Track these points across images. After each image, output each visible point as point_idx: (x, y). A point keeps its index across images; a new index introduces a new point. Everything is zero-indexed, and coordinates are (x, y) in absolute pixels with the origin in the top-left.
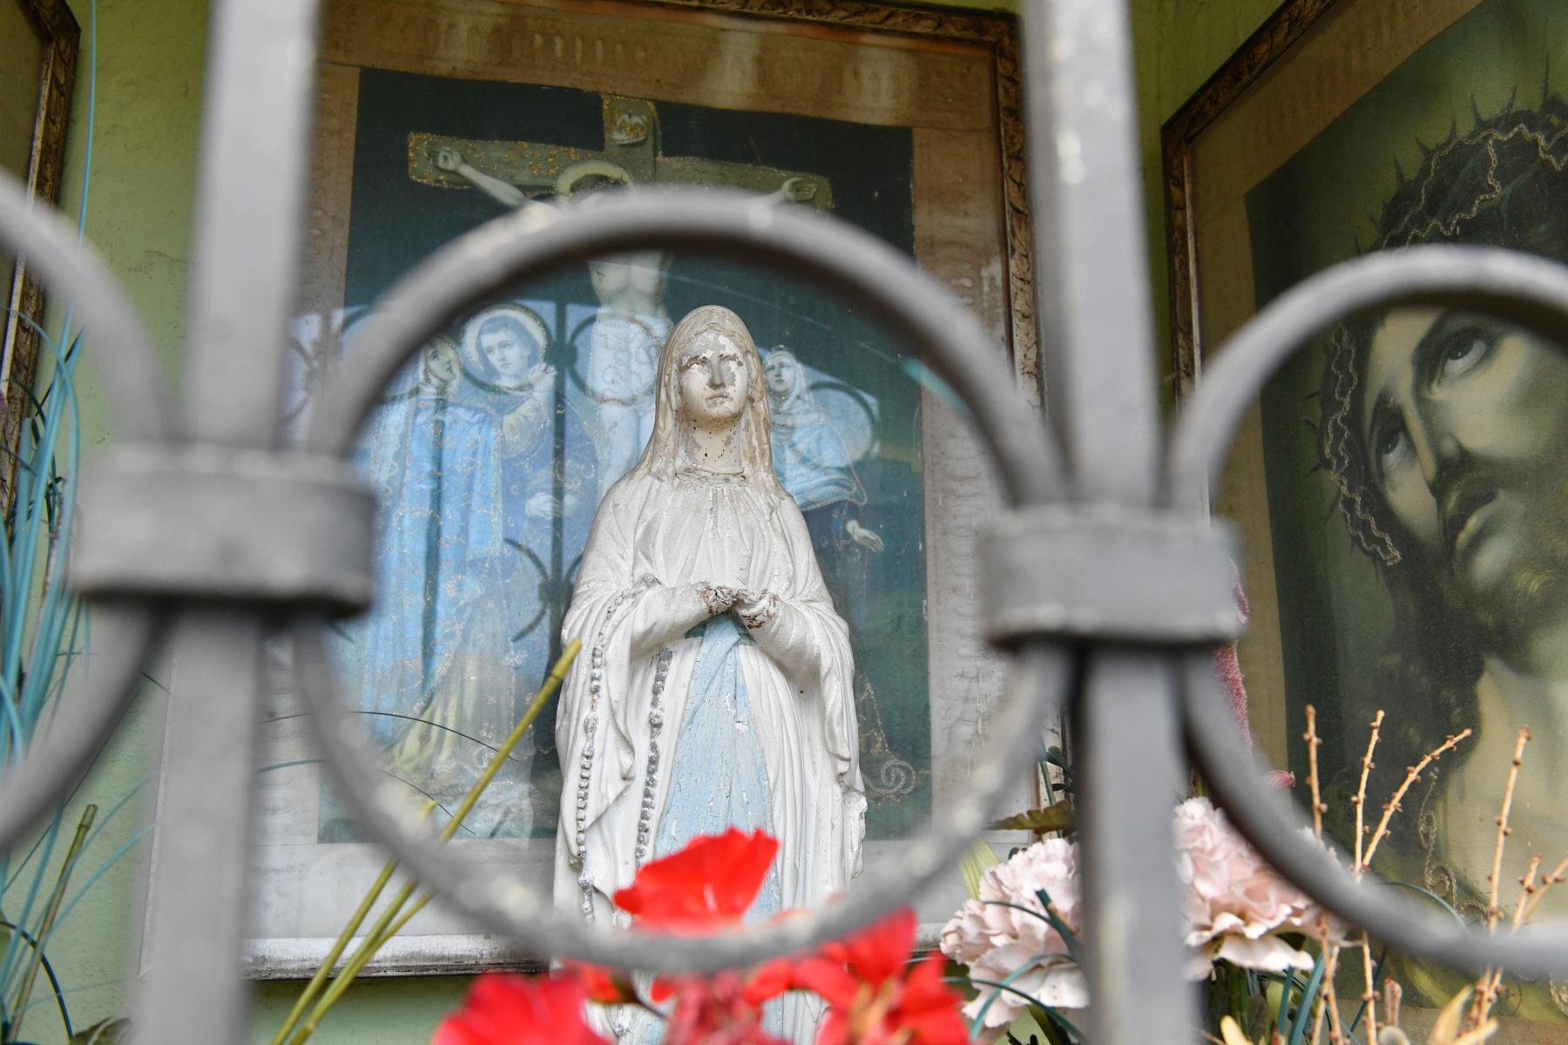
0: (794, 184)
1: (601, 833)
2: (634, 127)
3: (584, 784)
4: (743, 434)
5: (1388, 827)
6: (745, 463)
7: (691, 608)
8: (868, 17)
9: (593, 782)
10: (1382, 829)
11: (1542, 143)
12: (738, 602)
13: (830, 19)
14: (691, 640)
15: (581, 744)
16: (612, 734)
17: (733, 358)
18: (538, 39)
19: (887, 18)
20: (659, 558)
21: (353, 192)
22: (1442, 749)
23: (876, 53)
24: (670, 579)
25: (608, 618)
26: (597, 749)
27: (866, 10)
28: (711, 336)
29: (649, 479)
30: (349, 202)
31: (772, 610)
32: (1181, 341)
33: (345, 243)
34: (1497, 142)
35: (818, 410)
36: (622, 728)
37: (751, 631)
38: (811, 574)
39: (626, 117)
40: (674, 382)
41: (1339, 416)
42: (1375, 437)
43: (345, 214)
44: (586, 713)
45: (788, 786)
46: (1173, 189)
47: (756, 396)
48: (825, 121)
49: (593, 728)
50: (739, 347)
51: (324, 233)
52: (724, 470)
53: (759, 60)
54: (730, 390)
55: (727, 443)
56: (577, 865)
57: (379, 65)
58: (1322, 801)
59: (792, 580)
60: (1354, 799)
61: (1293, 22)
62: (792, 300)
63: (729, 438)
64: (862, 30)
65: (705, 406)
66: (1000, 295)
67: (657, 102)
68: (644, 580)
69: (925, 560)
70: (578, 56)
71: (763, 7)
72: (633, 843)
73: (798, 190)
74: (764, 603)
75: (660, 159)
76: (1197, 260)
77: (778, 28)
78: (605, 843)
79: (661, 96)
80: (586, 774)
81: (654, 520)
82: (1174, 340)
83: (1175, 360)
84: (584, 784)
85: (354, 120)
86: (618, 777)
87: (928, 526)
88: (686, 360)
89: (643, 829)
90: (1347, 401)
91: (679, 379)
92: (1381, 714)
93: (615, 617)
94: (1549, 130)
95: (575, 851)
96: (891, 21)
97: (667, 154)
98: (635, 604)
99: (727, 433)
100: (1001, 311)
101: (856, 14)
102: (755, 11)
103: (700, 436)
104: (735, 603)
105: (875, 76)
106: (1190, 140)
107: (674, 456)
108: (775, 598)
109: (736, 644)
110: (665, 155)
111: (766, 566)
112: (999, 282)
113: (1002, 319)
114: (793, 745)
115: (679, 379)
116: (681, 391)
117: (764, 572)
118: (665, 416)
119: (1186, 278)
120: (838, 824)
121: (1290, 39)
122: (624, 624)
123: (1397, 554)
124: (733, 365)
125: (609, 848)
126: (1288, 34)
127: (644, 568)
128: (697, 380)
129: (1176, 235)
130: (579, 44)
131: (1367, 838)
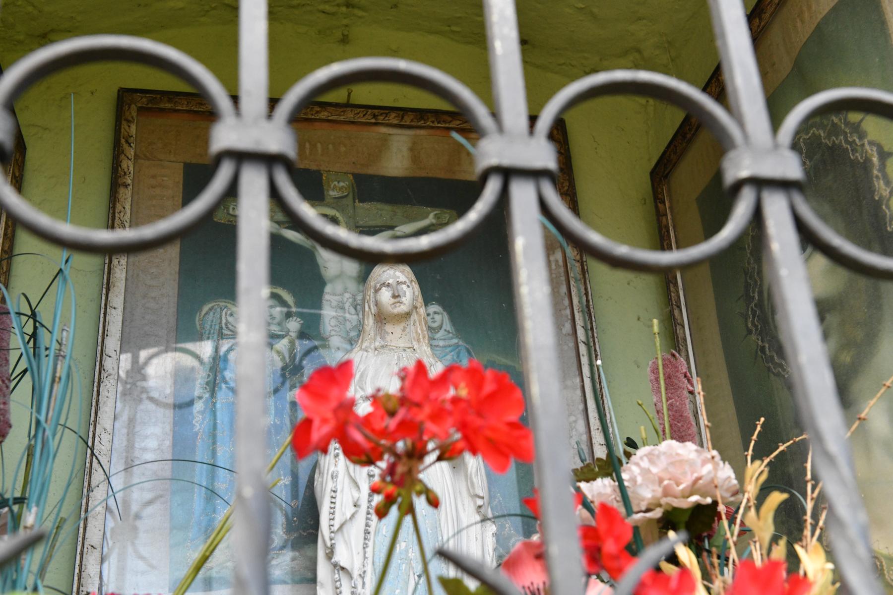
1: (343, 536)
2: (341, 189)
3: (333, 506)
6: (414, 343)
9: (338, 505)
15: (330, 485)
16: (347, 480)
17: (405, 283)
26: (339, 488)
29: (361, 352)
32: (672, 289)
34: (804, 139)
35: (457, 337)
36: (352, 474)
39: (336, 183)
40: (372, 299)
41: (753, 305)
44: (332, 469)
45: (448, 510)
47: (419, 305)
48: (452, 180)
49: (337, 476)
52: (402, 345)
53: (411, 149)
54: (403, 299)
55: (404, 330)
56: (330, 555)
57: (194, 161)
62: (438, 277)
65: (390, 309)
66: (562, 270)
67: (354, 175)
70: (308, 152)
71: (412, 121)
72: (362, 541)
73: (438, 218)
77: (422, 132)
78: (345, 541)
79: (356, 171)
80: (333, 500)
81: (365, 370)
82: (668, 289)
83: (670, 300)
84: (333, 506)
85: (181, 190)
86: (351, 505)
89: (367, 532)
92: (762, 419)
95: (329, 544)
97: (361, 201)
99: (402, 325)
100: (563, 278)
102: (408, 123)
103: (389, 328)
106: (666, 177)
107: (375, 340)
110: (360, 201)
112: (561, 263)
113: (564, 283)
114: (452, 496)
116: (377, 304)
120: (479, 538)
124: (404, 287)
125: (347, 543)
128: (385, 296)
130: (307, 145)
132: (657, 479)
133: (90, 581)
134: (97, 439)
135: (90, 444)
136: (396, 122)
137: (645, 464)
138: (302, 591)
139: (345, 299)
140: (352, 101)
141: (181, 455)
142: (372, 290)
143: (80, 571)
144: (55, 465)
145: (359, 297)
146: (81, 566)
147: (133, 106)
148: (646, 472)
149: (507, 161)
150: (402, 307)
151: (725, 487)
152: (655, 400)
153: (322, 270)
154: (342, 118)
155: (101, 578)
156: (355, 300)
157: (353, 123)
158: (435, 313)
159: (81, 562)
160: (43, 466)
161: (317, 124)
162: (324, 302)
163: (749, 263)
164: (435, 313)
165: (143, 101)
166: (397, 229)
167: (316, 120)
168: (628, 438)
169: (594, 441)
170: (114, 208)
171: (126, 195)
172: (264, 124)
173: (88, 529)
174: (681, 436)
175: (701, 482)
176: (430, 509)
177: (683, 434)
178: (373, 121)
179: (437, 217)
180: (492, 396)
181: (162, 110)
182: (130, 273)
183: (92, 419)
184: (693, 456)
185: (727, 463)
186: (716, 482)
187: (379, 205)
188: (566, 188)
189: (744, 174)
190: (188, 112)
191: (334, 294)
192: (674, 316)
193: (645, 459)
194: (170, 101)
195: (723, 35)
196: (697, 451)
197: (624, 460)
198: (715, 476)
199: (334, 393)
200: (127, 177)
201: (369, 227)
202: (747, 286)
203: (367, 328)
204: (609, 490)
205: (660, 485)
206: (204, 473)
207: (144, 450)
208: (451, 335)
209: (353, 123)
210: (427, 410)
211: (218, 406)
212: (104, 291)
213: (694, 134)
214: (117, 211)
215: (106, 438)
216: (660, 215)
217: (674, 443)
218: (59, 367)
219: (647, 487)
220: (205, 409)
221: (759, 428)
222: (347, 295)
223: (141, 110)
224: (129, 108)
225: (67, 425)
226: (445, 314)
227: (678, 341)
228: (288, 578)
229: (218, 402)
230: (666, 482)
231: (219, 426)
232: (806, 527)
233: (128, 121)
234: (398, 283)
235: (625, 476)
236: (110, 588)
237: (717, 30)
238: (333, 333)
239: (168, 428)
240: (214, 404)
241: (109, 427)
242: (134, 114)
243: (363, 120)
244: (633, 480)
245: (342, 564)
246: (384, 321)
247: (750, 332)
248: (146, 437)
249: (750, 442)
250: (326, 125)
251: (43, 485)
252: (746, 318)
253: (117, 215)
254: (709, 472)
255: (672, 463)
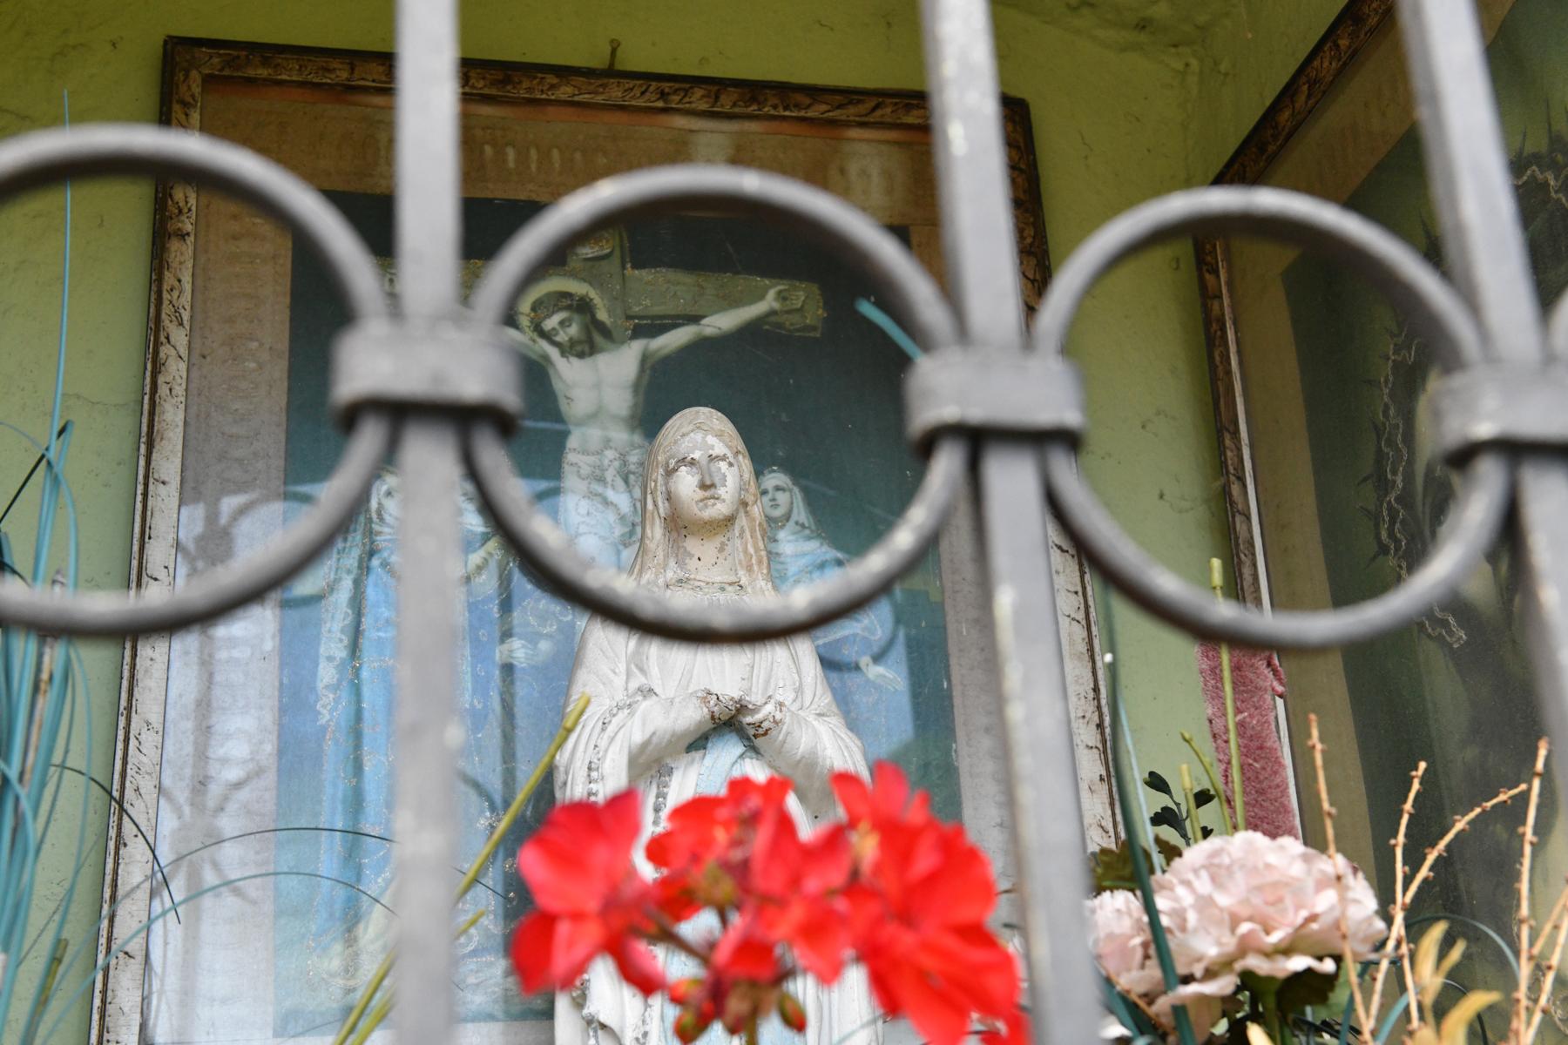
0: (780, 292)
4: (738, 542)
5: (1432, 869)
6: (741, 573)
7: (691, 716)
8: (852, 110)
10: (1424, 872)
11: (1552, 183)
12: (742, 708)
13: (810, 114)
14: (693, 754)
17: (724, 458)
18: (488, 150)
19: (874, 109)
20: (654, 670)
21: (292, 320)
22: (1494, 801)
23: (864, 148)
24: (666, 689)
25: (603, 730)
27: (851, 102)
28: (698, 436)
30: (287, 334)
31: (778, 716)
32: (1228, 442)
33: (285, 375)
37: (758, 742)
38: (819, 686)
40: (661, 488)
41: (1392, 497)
42: (1428, 511)
43: (284, 345)
46: (1207, 276)
47: (750, 499)
50: (730, 447)
51: (261, 366)
52: (718, 579)
54: (721, 491)
55: (721, 550)
58: (1332, 804)
59: (799, 691)
60: (1393, 842)
61: (1312, 84)
62: (784, 417)
63: (723, 544)
64: (847, 124)
65: (696, 510)
68: (640, 689)
69: (950, 698)
70: (533, 167)
71: (734, 105)
73: (785, 299)
74: (769, 708)
75: (629, 271)
76: (1239, 352)
77: (753, 126)
82: (1220, 449)
83: (1223, 464)
87: (953, 661)
88: (672, 463)
90: (1399, 479)
91: (666, 484)
92: (1423, 765)
93: (611, 729)
94: (1555, 167)
96: (879, 112)
97: (637, 265)
98: (631, 714)
99: (719, 539)
101: (840, 107)
102: (727, 109)
103: (692, 544)
104: (738, 710)
105: (864, 173)
107: (665, 568)
108: (781, 704)
109: (741, 756)
110: (634, 267)
111: (770, 677)
115: (666, 484)
116: (669, 497)
117: (767, 682)
118: (653, 524)
119: (1229, 372)
121: (1311, 102)
122: (620, 735)
123: (1462, 634)
124: (723, 465)
126: (1309, 96)
127: (638, 680)
128: (686, 483)
129: (1215, 326)
130: (533, 153)
131: (1408, 881)
132: (1226, 917)
133: (122, 1020)
134: (133, 743)
135: (116, 794)
136: (703, 106)
137: (1203, 885)
138: (528, 1032)
139: (606, 462)
140: (619, 67)
141: (294, 752)
142: (661, 471)
143: (104, 1002)
144: (39, 867)
145: (633, 458)
146: (104, 992)
147: (194, 74)
148: (1205, 903)
149: (977, 412)
150: (719, 506)
151: (1361, 935)
152: (1210, 711)
153: (563, 405)
154: (599, 99)
155: (147, 956)
156: (625, 463)
157: (622, 108)
158: (778, 488)
159: (105, 984)
160: (15, 875)
161: (551, 109)
162: (566, 468)
163: (1386, 413)
164: (778, 488)
165: (213, 63)
166: (704, 322)
167: (549, 102)
168: (1152, 774)
169: (1077, 740)
170: (160, 280)
171: (182, 255)
172: (459, 321)
173: (117, 919)
174: (1267, 822)
175: (1314, 926)
176: (788, 1034)
177: (1265, 785)
178: (660, 104)
179: (782, 297)
180: (931, 879)
181: (250, 81)
182: (193, 410)
183: (123, 703)
184: (1297, 869)
185: (1360, 875)
186: (1344, 928)
187: (672, 275)
188: (1029, 240)
189: (1484, 429)
190: (303, 84)
191: (585, 452)
192: (1230, 495)
193: (1204, 874)
194: (265, 62)
195: (1434, 98)
196: (1306, 858)
197: (1158, 859)
198: (1343, 913)
199: (600, 854)
200: (183, 218)
201: (653, 318)
202: (1380, 457)
203: (651, 545)
204: (1126, 925)
205: (1233, 930)
206: (340, 808)
207: (225, 761)
208: (807, 532)
209: (622, 108)
210: (797, 913)
211: (365, 674)
212: (143, 448)
213: (1282, 146)
214: (165, 287)
215: (149, 740)
216: (1207, 296)
217: (1258, 838)
218: (46, 659)
219: (1209, 933)
220: (340, 681)
221: (1416, 786)
222: (610, 454)
223: (209, 81)
224: (187, 76)
225: (68, 764)
226: (796, 490)
227: (1237, 545)
228: (497, 1010)
229: (365, 667)
230: (1245, 928)
231: (366, 715)
232: (1518, 1014)
233: (185, 104)
234: (711, 458)
235: (1161, 902)
236: (162, 1031)
237: (1419, 83)
238: (583, 529)
239: (269, 718)
240: (357, 672)
241: (156, 720)
242: (196, 90)
243: (641, 103)
244: (1180, 915)
245: (603, 1019)
246: (684, 532)
247: (1384, 550)
248: (228, 736)
249: (1401, 817)
250: (570, 110)
251: (17, 906)
252: (1376, 519)
253: (166, 296)
254: (1332, 908)
255: (1259, 889)
